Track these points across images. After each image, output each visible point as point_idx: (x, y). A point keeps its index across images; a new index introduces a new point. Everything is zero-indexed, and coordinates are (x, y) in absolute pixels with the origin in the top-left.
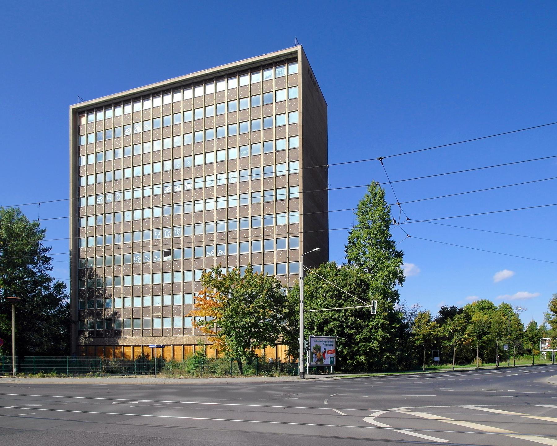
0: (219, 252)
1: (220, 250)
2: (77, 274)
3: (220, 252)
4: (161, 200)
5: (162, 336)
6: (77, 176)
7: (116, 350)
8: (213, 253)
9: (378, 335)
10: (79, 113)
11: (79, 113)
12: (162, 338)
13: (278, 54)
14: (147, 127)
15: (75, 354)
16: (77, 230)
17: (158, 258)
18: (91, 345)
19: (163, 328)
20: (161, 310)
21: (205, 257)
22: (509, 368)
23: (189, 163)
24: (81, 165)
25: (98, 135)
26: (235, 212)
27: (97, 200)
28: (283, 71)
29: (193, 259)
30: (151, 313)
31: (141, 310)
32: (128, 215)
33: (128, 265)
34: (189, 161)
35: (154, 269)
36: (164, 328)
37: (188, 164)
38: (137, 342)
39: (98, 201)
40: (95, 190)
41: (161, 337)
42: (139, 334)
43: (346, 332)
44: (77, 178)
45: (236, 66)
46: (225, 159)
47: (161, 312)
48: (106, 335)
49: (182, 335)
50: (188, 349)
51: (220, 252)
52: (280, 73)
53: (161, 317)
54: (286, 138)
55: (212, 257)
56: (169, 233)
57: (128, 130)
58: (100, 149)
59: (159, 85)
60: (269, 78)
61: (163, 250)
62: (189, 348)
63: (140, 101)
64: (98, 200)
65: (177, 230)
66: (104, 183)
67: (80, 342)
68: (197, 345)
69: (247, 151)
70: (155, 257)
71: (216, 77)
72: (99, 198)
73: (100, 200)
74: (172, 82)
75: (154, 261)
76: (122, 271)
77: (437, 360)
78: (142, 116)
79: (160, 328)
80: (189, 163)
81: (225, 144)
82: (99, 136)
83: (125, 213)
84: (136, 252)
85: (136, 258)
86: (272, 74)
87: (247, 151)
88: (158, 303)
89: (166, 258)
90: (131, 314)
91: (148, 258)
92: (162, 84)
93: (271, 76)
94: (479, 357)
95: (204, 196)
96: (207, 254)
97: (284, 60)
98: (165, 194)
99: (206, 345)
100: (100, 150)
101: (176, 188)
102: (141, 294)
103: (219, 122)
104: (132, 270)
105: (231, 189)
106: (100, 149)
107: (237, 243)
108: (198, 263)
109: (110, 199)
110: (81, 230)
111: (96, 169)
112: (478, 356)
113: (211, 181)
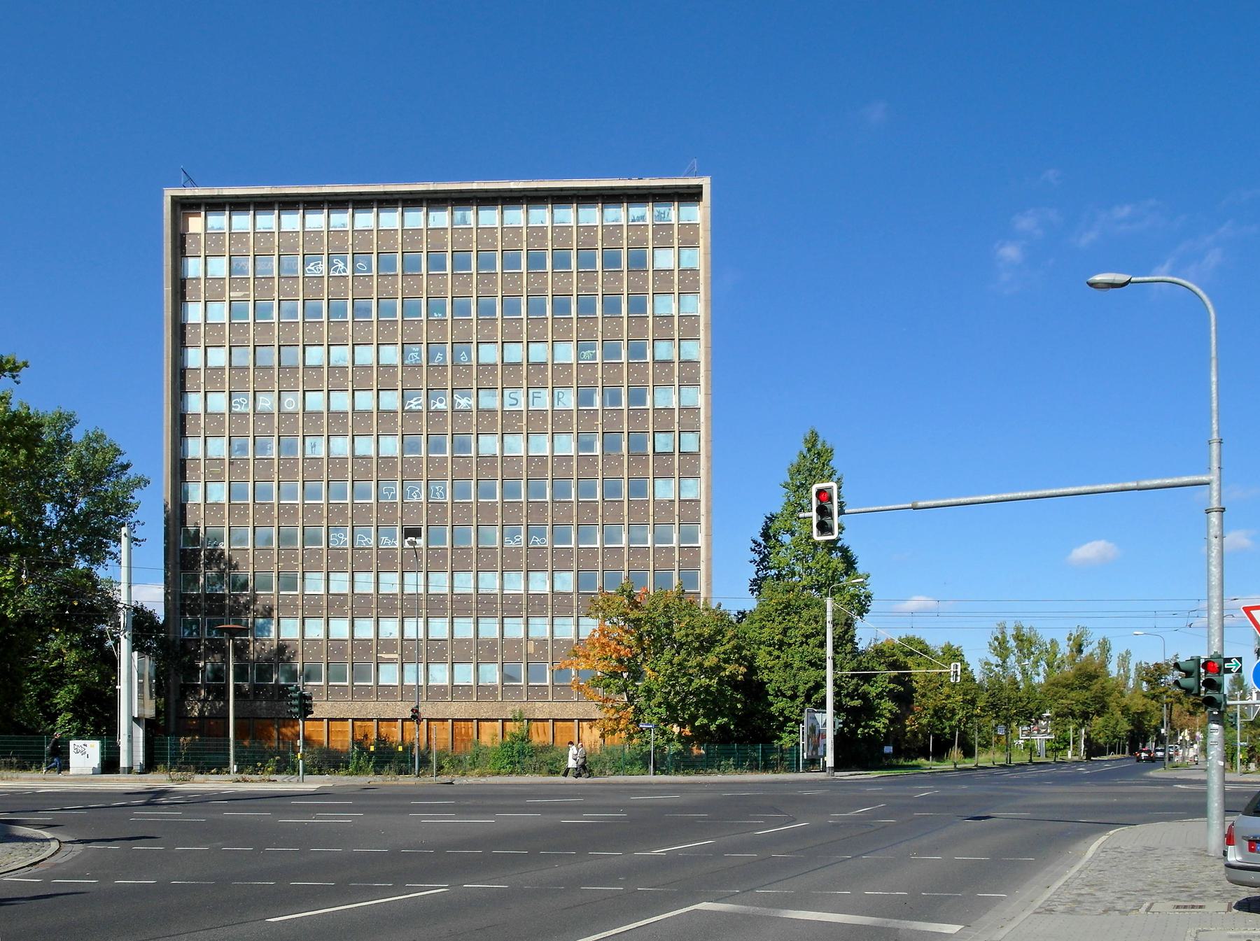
2: (178, 560)
3: (535, 539)
4: (400, 423)
5: (402, 701)
6: (179, 345)
7: (284, 730)
8: (518, 540)
9: (885, 709)
10: (185, 206)
11: (185, 206)
13: (690, 184)
16: (179, 462)
17: (396, 542)
18: (218, 716)
19: (402, 684)
20: (399, 648)
22: (993, 768)
23: (463, 356)
25: (234, 264)
26: (570, 468)
27: (233, 402)
28: (674, 213)
29: (475, 548)
30: (375, 652)
31: (350, 645)
32: (315, 446)
34: (464, 353)
35: (385, 560)
36: (405, 684)
37: (462, 358)
38: (341, 713)
39: (233, 404)
40: (227, 379)
41: (399, 703)
42: (344, 695)
43: (844, 703)
44: (179, 348)
46: (521, 361)
47: (399, 652)
48: (255, 695)
49: (449, 699)
50: (461, 729)
51: (535, 539)
52: (663, 215)
53: (399, 661)
56: (417, 491)
57: (316, 264)
58: (242, 293)
60: (639, 221)
61: (403, 526)
62: (464, 724)
63: (200, 216)
64: (234, 403)
65: (437, 488)
66: (251, 370)
67: (187, 711)
68: (510, 720)
69: (594, 352)
70: (383, 538)
71: (527, 197)
72: (238, 400)
73: (240, 403)
74: (431, 189)
75: (380, 547)
76: (300, 561)
77: (888, 751)
78: (351, 243)
79: (397, 684)
80: (463, 356)
82: (238, 265)
83: (307, 438)
84: (336, 524)
85: (334, 537)
86: (646, 213)
88: (391, 634)
90: (325, 652)
91: (366, 539)
93: (643, 218)
94: (958, 746)
95: (500, 427)
97: (670, 194)
98: (407, 411)
99: (529, 720)
100: (242, 297)
101: (434, 404)
102: (350, 612)
103: (534, 287)
104: (325, 560)
105: (559, 419)
107: (323, 528)
108: (486, 557)
110: (189, 465)
112: (956, 747)
113: (341, 402)
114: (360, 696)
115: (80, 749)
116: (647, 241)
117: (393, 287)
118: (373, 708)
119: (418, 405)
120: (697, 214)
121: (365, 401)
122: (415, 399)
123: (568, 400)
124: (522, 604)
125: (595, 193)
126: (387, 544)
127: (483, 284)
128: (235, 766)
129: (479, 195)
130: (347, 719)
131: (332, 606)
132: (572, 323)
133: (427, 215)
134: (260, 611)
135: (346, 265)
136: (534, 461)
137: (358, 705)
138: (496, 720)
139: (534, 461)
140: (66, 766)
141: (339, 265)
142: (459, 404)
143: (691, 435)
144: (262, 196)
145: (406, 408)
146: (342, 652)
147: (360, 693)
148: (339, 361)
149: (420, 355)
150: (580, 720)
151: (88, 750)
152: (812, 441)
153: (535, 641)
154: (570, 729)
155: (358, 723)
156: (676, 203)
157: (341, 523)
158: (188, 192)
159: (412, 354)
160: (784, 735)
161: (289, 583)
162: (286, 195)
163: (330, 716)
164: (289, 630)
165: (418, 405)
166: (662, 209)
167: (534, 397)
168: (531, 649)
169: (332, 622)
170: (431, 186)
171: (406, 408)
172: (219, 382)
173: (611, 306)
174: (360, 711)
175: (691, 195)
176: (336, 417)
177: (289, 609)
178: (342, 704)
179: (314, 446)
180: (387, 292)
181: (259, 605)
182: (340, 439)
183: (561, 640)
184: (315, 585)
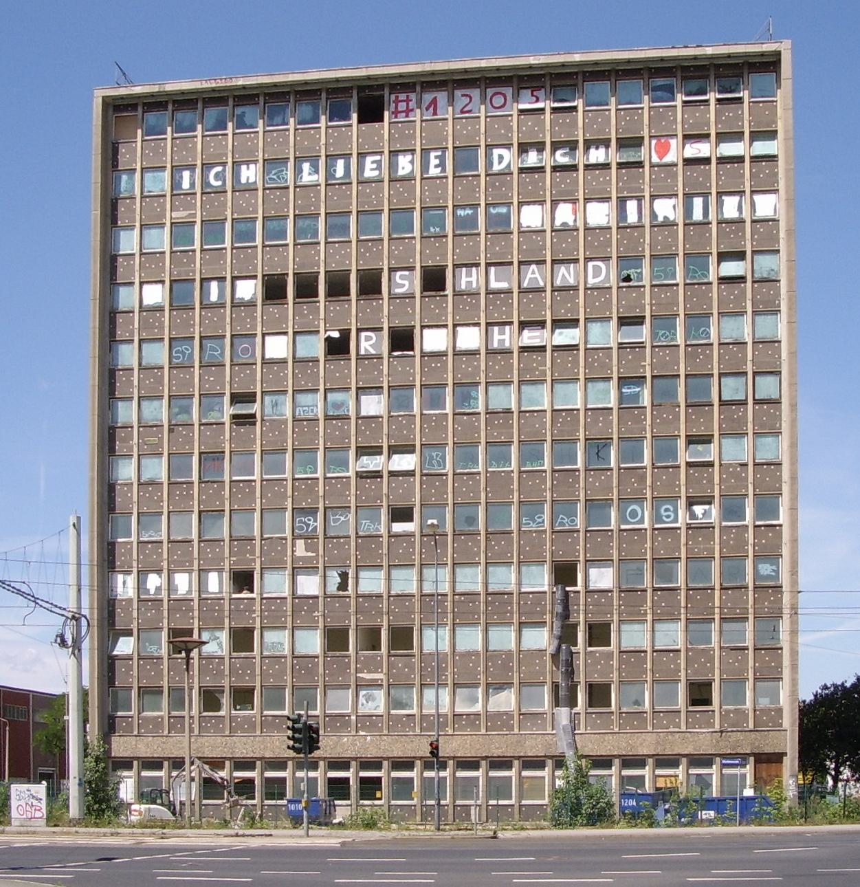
0: (559, 520)
1: (561, 516)
12: (390, 740)
14: (500, 163)
15: (773, 574)
21: (520, 530)
24: (121, 253)
33: (277, 538)
39: (174, 354)
45: (616, 60)
51: (562, 518)
54: (162, 339)
55: (539, 531)
58: (185, 213)
59: (470, 66)
61: (389, 506)
69: (639, 271)
70: (364, 522)
81: (578, 246)
87: (639, 271)
89: (398, 527)
92: (398, 72)
96: (524, 522)
106: (185, 213)
108: (498, 544)
109: (216, 353)
111: (170, 268)
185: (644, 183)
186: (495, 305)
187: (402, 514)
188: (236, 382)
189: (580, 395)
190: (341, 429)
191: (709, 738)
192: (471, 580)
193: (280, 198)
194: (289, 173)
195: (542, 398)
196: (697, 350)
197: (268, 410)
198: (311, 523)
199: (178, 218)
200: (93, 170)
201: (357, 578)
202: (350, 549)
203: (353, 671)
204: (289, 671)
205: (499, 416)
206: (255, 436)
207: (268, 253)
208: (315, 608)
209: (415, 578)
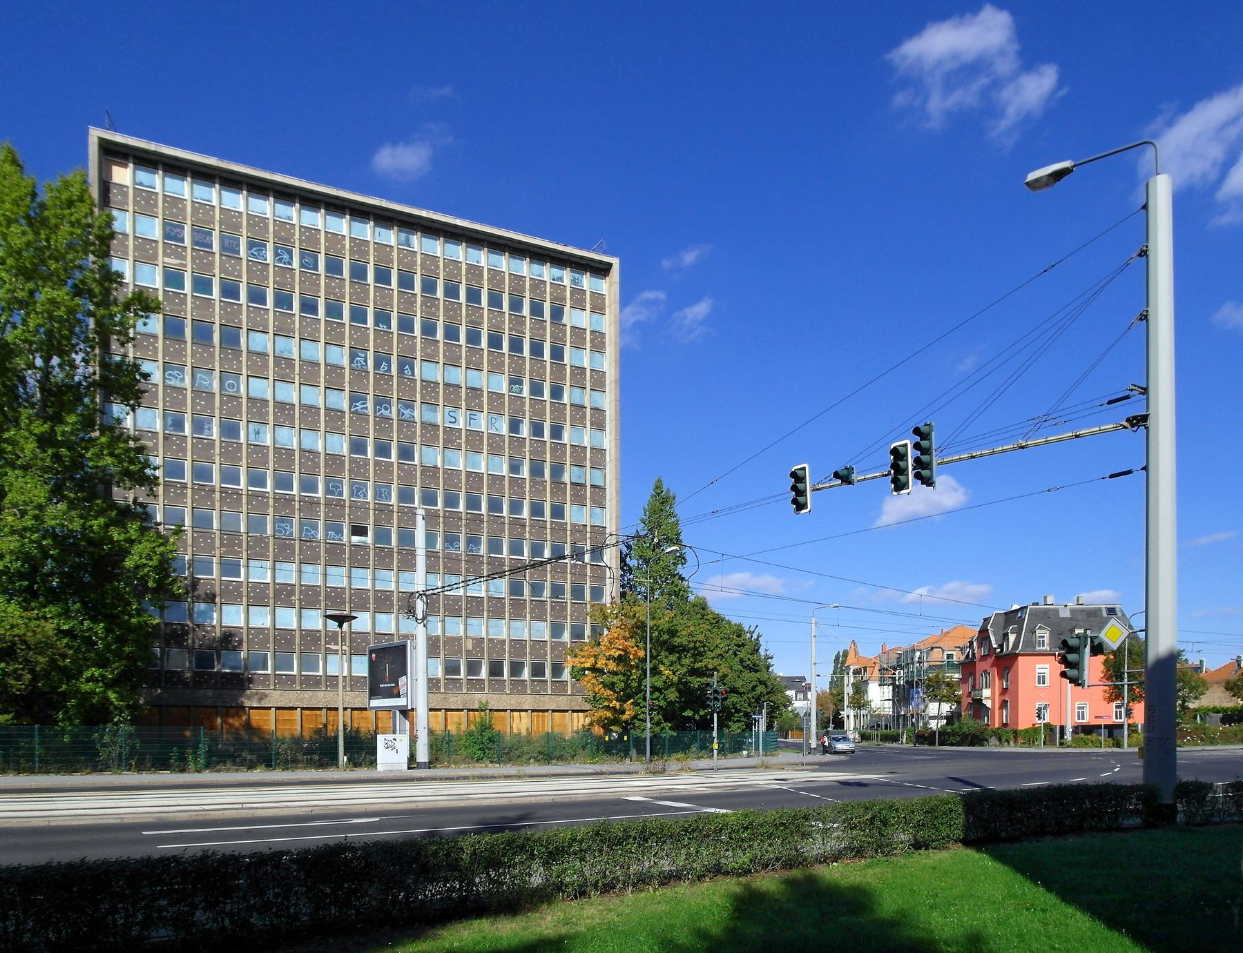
11: (112, 153)
28: (587, 282)
41: (349, 693)
57: (259, 250)
89: (355, 539)
114: (309, 686)
115: (390, 743)
116: (565, 300)
117: (340, 290)
118: (321, 698)
119: (364, 408)
120: (608, 287)
121: (314, 396)
122: (360, 402)
123: (342, 401)
124: (461, 605)
125: (439, 227)
126: (334, 539)
127: (427, 307)
128: (345, 758)
129: (532, 249)
130: (296, 708)
131: (258, 596)
132: (320, 325)
133: (247, 199)
134: (202, 597)
135: (291, 258)
136: (472, 477)
137: (308, 694)
138: (440, 710)
139: (472, 477)
140: (373, 763)
141: (284, 257)
142: (403, 414)
143: (598, 471)
144: (205, 166)
145: (352, 410)
146: (290, 642)
147: (312, 683)
148: (283, 352)
149: (366, 361)
150: (512, 711)
151: (397, 744)
152: (658, 486)
153: (473, 639)
154: (503, 718)
155: (307, 712)
156: (372, 223)
157: (288, 513)
158: (119, 138)
159: (358, 359)
160: (730, 724)
161: (230, 568)
162: (233, 172)
163: (279, 705)
164: (232, 617)
165: (364, 408)
166: (577, 276)
167: (470, 419)
168: (470, 647)
169: (277, 610)
170: (384, 203)
171: (352, 410)
172: (150, 350)
173: (537, 350)
174: (310, 700)
175: (601, 270)
176: (283, 408)
177: (232, 595)
178: (291, 693)
179: (257, 433)
180: (335, 295)
181: (201, 591)
182: (285, 430)
183: (494, 639)
184: (260, 573)
185: (525, 328)
186: (426, 390)
187: (359, 531)
188: (224, 410)
189: (505, 630)
190: (313, 460)
191: (565, 699)
192: (288, 574)
193: (262, 271)
194: (268, 253)
195: (460, 462)
196: (558, 449)
197: (252, 436)
198: (288, 528)
199: (169, 264)
200: (202, 312)
201: (248, 566)
202: (320, 551)
203: (323, 643)
204: (271, 640)
205: (430, 472)
206: (242, 455)
207: (251, 312)
208: (292, 593)
209: (393, 579)
